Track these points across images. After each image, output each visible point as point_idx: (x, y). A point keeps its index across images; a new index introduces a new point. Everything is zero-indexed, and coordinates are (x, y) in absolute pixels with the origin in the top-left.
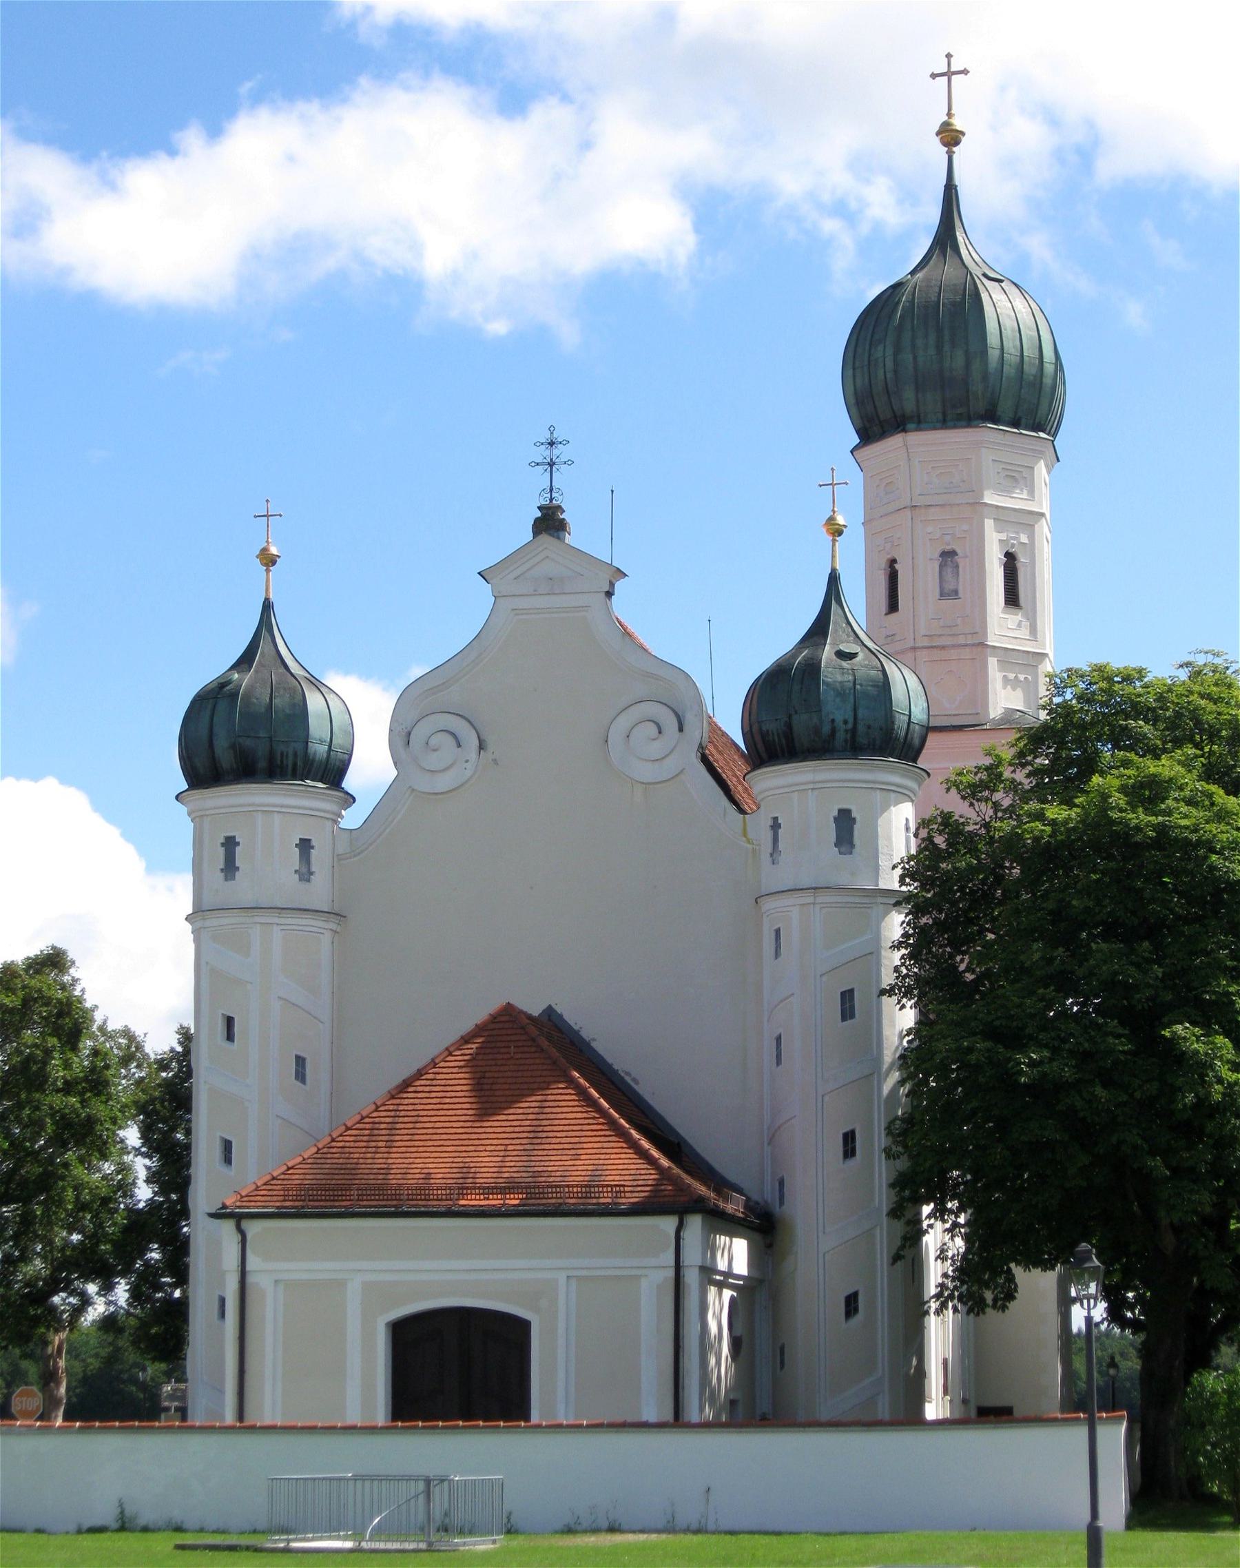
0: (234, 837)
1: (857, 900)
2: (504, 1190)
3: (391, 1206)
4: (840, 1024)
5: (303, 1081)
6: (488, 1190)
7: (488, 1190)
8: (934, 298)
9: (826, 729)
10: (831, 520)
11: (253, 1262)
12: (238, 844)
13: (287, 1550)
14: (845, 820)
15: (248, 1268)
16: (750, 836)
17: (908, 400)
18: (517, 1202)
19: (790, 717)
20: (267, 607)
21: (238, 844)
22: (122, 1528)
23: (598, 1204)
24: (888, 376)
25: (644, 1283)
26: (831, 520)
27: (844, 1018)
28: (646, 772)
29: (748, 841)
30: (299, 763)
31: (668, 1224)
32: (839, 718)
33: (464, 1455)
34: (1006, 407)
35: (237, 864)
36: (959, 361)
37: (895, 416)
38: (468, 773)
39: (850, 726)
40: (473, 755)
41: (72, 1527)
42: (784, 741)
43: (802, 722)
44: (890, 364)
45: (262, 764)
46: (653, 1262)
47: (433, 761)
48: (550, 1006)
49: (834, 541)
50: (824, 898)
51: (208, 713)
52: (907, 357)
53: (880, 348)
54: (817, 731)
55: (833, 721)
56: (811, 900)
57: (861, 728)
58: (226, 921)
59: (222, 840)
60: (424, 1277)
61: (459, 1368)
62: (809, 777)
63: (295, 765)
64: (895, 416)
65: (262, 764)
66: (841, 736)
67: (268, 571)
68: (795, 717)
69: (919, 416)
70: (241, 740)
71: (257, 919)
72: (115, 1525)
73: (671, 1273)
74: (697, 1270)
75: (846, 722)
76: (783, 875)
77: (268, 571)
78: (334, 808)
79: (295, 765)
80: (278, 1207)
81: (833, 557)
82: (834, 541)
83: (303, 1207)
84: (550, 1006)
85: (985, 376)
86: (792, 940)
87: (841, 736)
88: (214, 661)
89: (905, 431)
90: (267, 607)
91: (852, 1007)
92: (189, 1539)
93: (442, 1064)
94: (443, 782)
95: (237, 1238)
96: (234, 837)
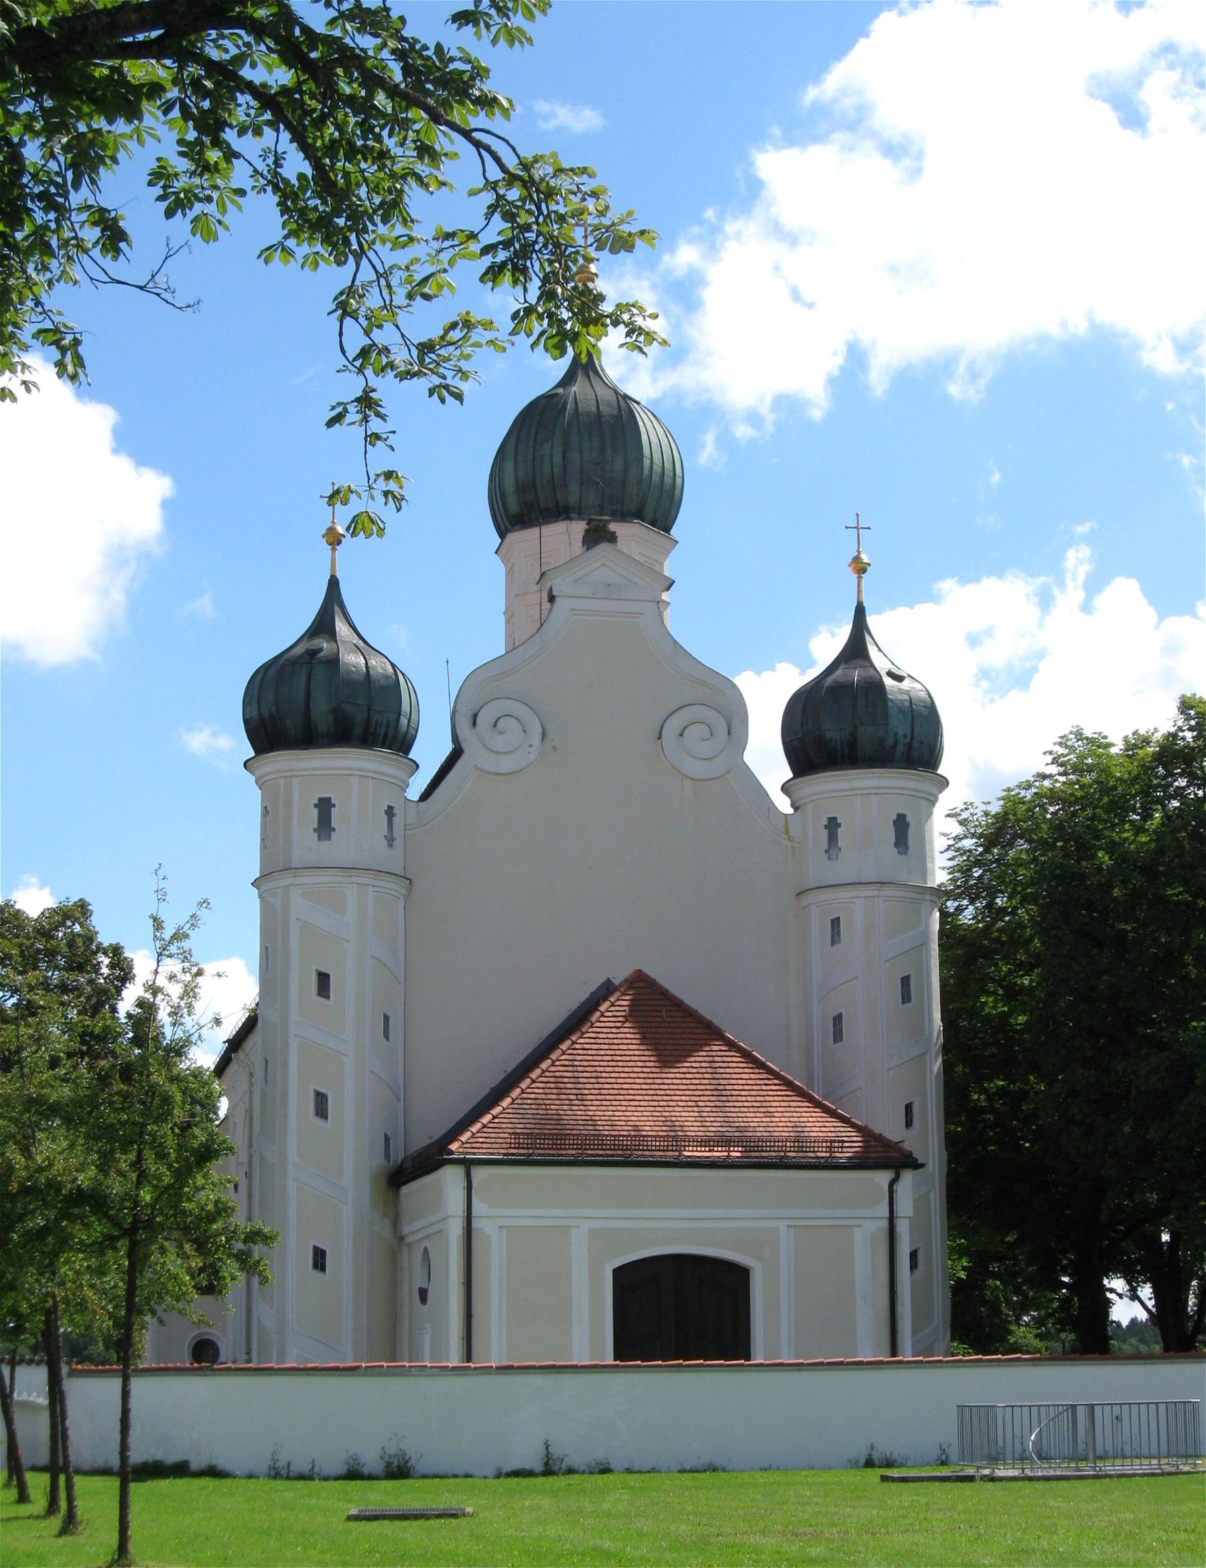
0: (330, 799)
1: (914, 896)
2: (726, 1142)
3: (618, 1156)
4: (901, 1007)
5: (387, 1039)
6: (705, 1143)
7: (705, 1143)
8: (594, 409)
9: (890, 742)
10: (857, 559)
11: (478, 1208)
12: (334, 805)
13: (992, 1479)
14: (901, 824)
15: (474, 1214)
16: (791, 834)
17: (573, 493)
18: (739, 1154)
19: (856, 727)
20: (334, 583)
21: (334, 805)
22: (548, 1471)
23: (818, 1157)
24: (556, 470)
25: (858, 1235)
26: (857, 559)
27: (903, 1002)
28: (696, 769)
29: (789, 839)
30: (390, 734)
31: (882, 1178)
32: (901, 733)
33: (683, 1399)
34: (649, 511)
35: (333, 825)
36: (619, 465)
37: (558, 506)
38: (532, 757)
39: (908, 740)
40: (536, 741)
41: (490, 1471)
42: (846, 749)
43: (866, 734)
44: (557, 458)
45: (358, 730)
46: (869, 1213)
47: (499, 742)
48: (609, 980)
49: (860, 578)
50: (887, 892)
51: (303, 678)
52: (575, 456)
53: (547, 446)
54: (882, 742)
55: (896, 734)
56: (876, 893)
57: (916, 744)
58: (324, 879)
59: (316, 801)
60: (651, 1224)
61: (681, 1311)
62: (873, 783)
63: (386, 734)
64: (558, 506)
65: (358, 730)
66: (900, 748)
67: (334, 550)
68: (861, 730)
69: (580, 508)
70: (343, 706)
71: (354, 879)
72: (539, 1467)
73: (885, 1224)
74: (907, 1221)
75: (905, 736)
76: (846, 867)
77: (334, 550)
78: (402, 775)
79: (386, 734)
80: (504, 1155)
81: (859, 591)
82: (860, 578)
83: (530, 1155)
84: (609, 980)
85: (640, 480)
86: (853, 931)
87: (900, 748)
88: (284, 631)
89: (568, 518)
90: (334, 583)
91: (909, 992)
92: (895, 1473)
93: (598, 1024)
94: (507, 764)
95: (462, 1184)
96: (330, 799)
